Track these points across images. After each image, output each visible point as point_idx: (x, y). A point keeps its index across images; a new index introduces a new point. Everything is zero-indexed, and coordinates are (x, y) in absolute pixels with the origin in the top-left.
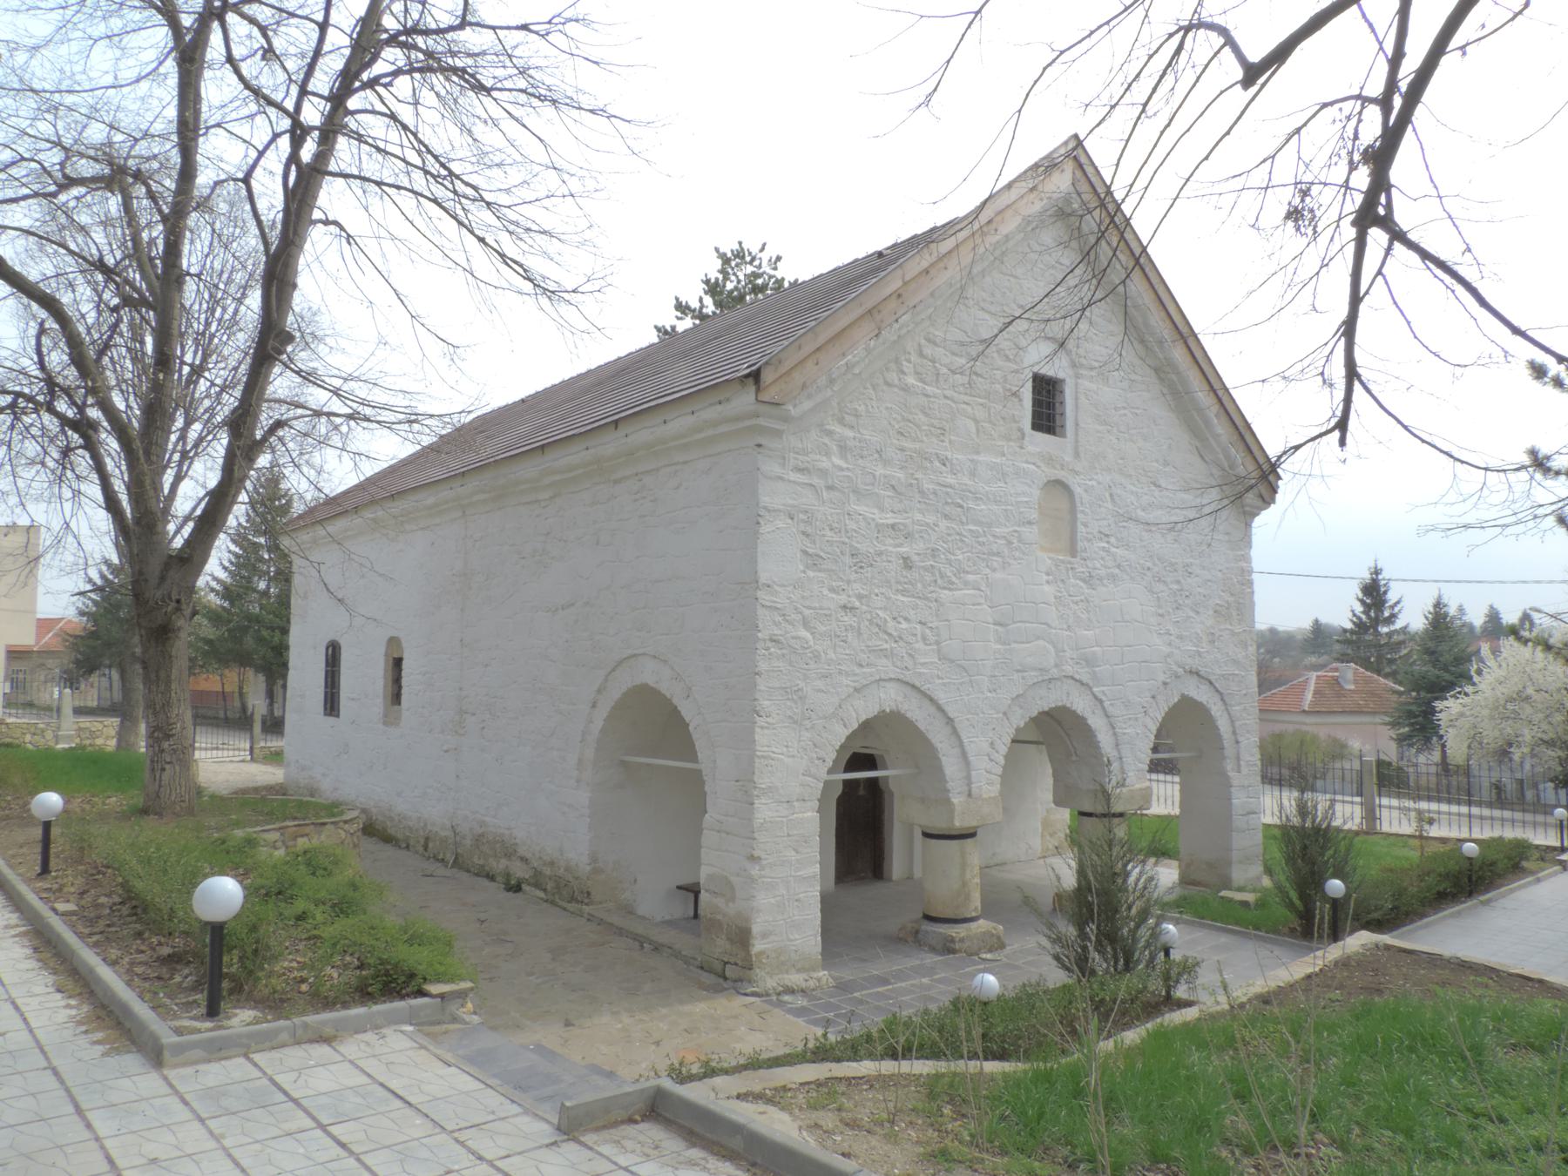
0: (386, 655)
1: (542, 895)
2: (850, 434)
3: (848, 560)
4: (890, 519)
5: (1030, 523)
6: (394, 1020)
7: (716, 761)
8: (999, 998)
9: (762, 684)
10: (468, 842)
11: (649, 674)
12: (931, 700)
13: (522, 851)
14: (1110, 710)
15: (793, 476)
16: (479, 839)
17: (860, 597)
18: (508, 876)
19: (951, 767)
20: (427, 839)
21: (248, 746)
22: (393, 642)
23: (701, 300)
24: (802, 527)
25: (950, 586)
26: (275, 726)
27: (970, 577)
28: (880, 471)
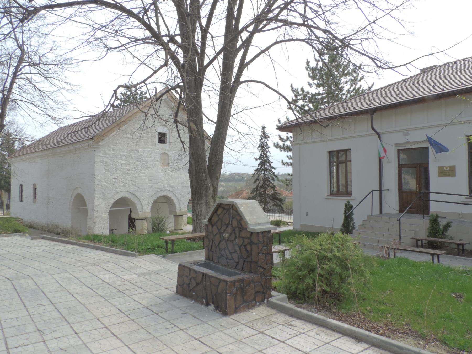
0: (33, 187)
1: (63, 235)
2: (115, 147)
3: (115, 170)
4: (124, 162)
5: (158, 161)
6: (17, 235)
7: (89, 206)
8: (287, 295)
9: (96, 192)
10: (50, 226)
11: (80, 191)
12: (134, 195)
13: (60, 227)
14: (177, 196)
15: (102, 155)
16: (52, 225)
17: (117, 176)
18: (58, 232)
19: (139, 207)
20: (42, 227)
21: (2, 212)
22: (34, 185)
23: (121, 97)
24: (104, 164)
25: (138, 174)
26: (8, 207)
27: (143, 172)
28: (122, 153)
